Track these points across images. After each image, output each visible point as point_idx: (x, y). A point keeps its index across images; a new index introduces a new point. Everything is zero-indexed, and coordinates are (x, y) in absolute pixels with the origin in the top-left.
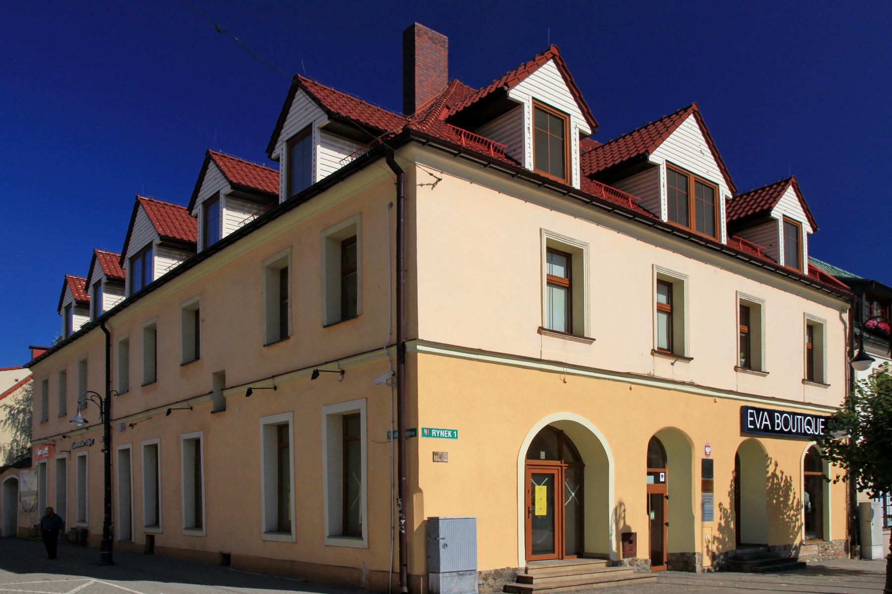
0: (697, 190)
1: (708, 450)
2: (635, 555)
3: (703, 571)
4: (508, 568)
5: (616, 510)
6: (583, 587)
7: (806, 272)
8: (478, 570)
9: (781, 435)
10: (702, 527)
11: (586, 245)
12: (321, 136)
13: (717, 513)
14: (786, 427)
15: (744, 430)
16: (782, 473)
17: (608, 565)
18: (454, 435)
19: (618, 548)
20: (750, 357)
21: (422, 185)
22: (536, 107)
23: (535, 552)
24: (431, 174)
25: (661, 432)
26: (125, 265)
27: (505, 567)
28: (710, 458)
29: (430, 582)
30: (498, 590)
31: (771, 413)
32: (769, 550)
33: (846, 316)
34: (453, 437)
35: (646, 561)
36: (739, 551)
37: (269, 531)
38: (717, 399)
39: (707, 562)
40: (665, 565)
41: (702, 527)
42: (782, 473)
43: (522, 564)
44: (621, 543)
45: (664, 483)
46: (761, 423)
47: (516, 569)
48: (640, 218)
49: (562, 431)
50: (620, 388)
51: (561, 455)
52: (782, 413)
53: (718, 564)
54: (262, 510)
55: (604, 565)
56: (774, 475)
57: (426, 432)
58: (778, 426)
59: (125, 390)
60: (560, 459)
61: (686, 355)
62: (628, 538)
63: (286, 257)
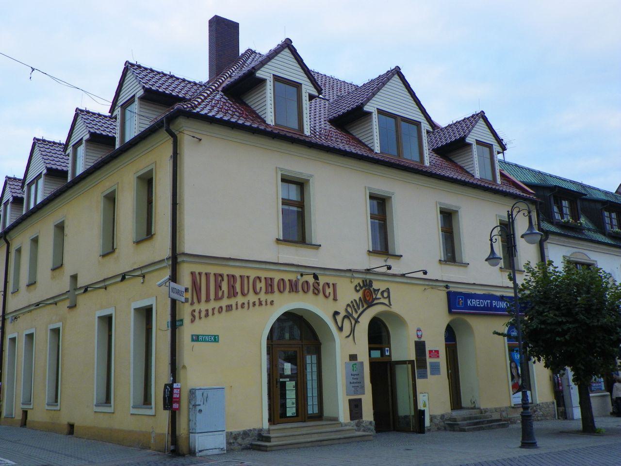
2: (361, 417)
4: (254, 429)
11: (312, 176)
12: (140, 104)
20: (451, 254)
22: (275, 78)
23: (432, 417)
24: (194, 137)
26: (24, 189)
27: (251, 428)
28: (422, 339)
29: (191, 441)
32: (481, 413)
35: (371, 423)
43: (266, 425)
47: (261, 430)
51: (296, 341)
54: (93, 389)
59: (16, 291)
63: (151, 170)
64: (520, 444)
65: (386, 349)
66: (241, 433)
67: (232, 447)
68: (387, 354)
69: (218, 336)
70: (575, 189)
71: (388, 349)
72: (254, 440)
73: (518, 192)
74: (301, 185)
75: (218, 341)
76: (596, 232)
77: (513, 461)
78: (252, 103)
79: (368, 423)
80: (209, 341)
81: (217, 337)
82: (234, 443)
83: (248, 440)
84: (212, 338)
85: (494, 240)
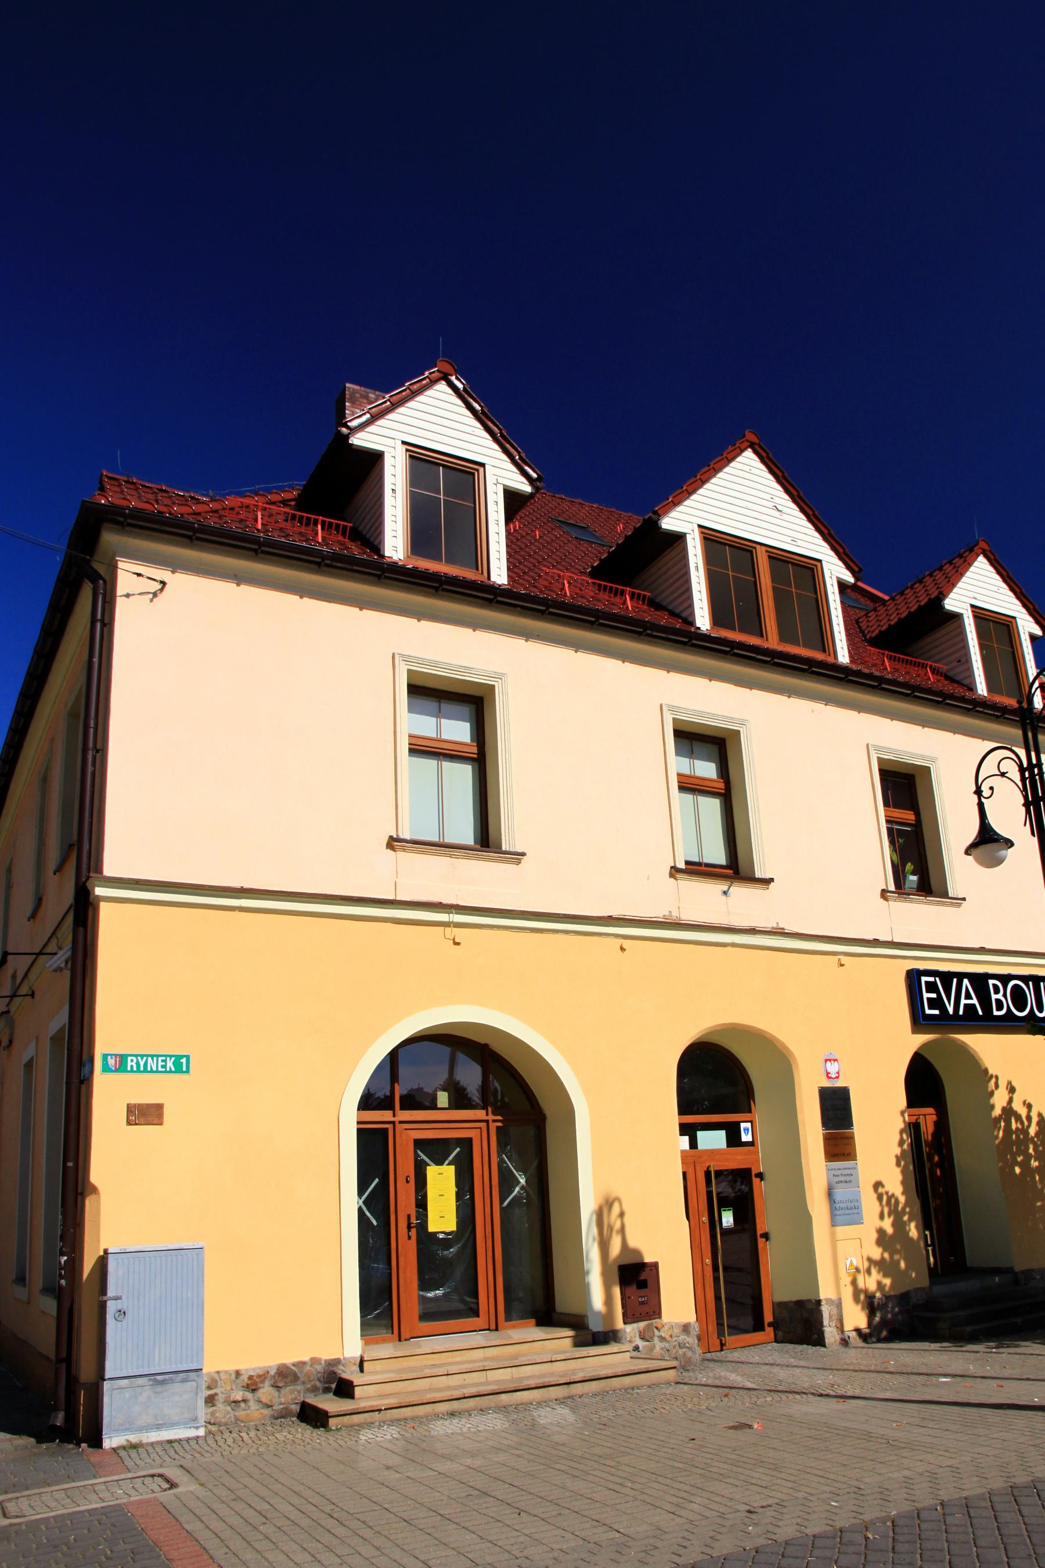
0: (775, 577)
2: (657, 1313)
3: (845, 1342)
4: (315, 1361)
5: (600, 1215)
6: (471, 1403)
8: (209, 1368)
9: (1008, 1024)
10: (834, 1242)
11: (500, 676)
13: (870, 1206)
14: (1021, 1007)
15: (919, 1021)
16: (1029, 1107)
17: (578, 1343)
18: (180, 1065)
19: (609, 1301)
21: (128, 596)
24: (139, 575)
25: (920, 1048)
28: (840, 1083)
30: (284, 1414)
31: (979, 981)
34: (178, 1069)
35: (686, 1328)
36: (938, 1289)
37: (25, 1286)
38: (844, 959)
39: (856, 1318)
40: (770, 1331)
41: (834, 1242)
42: (1029, 1107)
44: (617, 1291)
45: (751, 1144)
47: (338, 1361)
49: (486, 1045)
50: (599, 948)
52: (1005, 979)
53: (884, 1322)
55: (568, 1342)
56: (1008, 1112)
57: (111, 1062)
58: (1000, 1006)
60: (485, 1108)
62: (635, 1277)
65: (743, 1125)
66: (272, 1373)
67: (241, 1413)
69: (188, 1057)
71: (749, 1125)
72: (314, 1390)
74: (475, 702)
75: (188, 1071)
78: (677, 602)
79: (676, 1331)
80: (157, 1071)
81: (184, 1060)
82: (244, 1401)
83: (292, 1392)
84: (170, 1064)
85: (986, 792)
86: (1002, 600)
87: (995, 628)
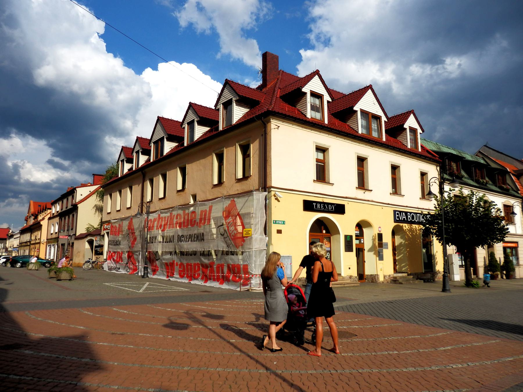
1: (380, 229)
7: (420, 150)
15: (396, 221)
18: (284, 223)
31: (406, 213)
33: (438, 168)
36: (395, 275)
46: (401, 217)
48: (352, 136)
52: (411, 213)
61: (181, 121)
64: (441, 290)
68: (362, 242)
70: (455, 153)
73: (430, 156)
76: (492, 185)
77: (356, 300)
86: (416, 126)
87: (413, 131)
